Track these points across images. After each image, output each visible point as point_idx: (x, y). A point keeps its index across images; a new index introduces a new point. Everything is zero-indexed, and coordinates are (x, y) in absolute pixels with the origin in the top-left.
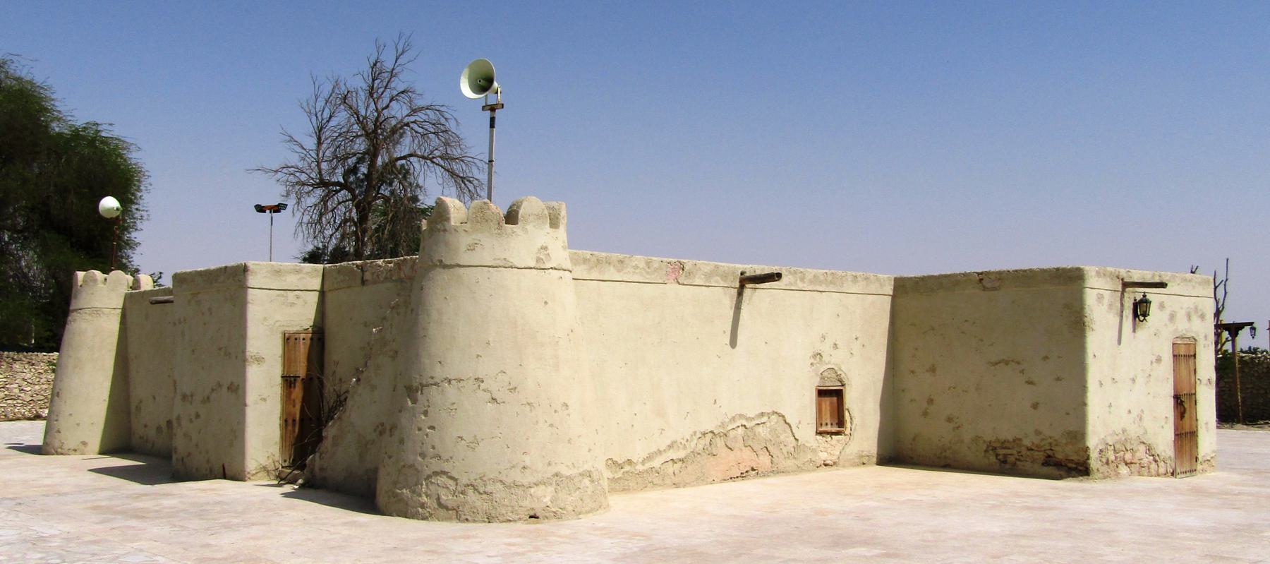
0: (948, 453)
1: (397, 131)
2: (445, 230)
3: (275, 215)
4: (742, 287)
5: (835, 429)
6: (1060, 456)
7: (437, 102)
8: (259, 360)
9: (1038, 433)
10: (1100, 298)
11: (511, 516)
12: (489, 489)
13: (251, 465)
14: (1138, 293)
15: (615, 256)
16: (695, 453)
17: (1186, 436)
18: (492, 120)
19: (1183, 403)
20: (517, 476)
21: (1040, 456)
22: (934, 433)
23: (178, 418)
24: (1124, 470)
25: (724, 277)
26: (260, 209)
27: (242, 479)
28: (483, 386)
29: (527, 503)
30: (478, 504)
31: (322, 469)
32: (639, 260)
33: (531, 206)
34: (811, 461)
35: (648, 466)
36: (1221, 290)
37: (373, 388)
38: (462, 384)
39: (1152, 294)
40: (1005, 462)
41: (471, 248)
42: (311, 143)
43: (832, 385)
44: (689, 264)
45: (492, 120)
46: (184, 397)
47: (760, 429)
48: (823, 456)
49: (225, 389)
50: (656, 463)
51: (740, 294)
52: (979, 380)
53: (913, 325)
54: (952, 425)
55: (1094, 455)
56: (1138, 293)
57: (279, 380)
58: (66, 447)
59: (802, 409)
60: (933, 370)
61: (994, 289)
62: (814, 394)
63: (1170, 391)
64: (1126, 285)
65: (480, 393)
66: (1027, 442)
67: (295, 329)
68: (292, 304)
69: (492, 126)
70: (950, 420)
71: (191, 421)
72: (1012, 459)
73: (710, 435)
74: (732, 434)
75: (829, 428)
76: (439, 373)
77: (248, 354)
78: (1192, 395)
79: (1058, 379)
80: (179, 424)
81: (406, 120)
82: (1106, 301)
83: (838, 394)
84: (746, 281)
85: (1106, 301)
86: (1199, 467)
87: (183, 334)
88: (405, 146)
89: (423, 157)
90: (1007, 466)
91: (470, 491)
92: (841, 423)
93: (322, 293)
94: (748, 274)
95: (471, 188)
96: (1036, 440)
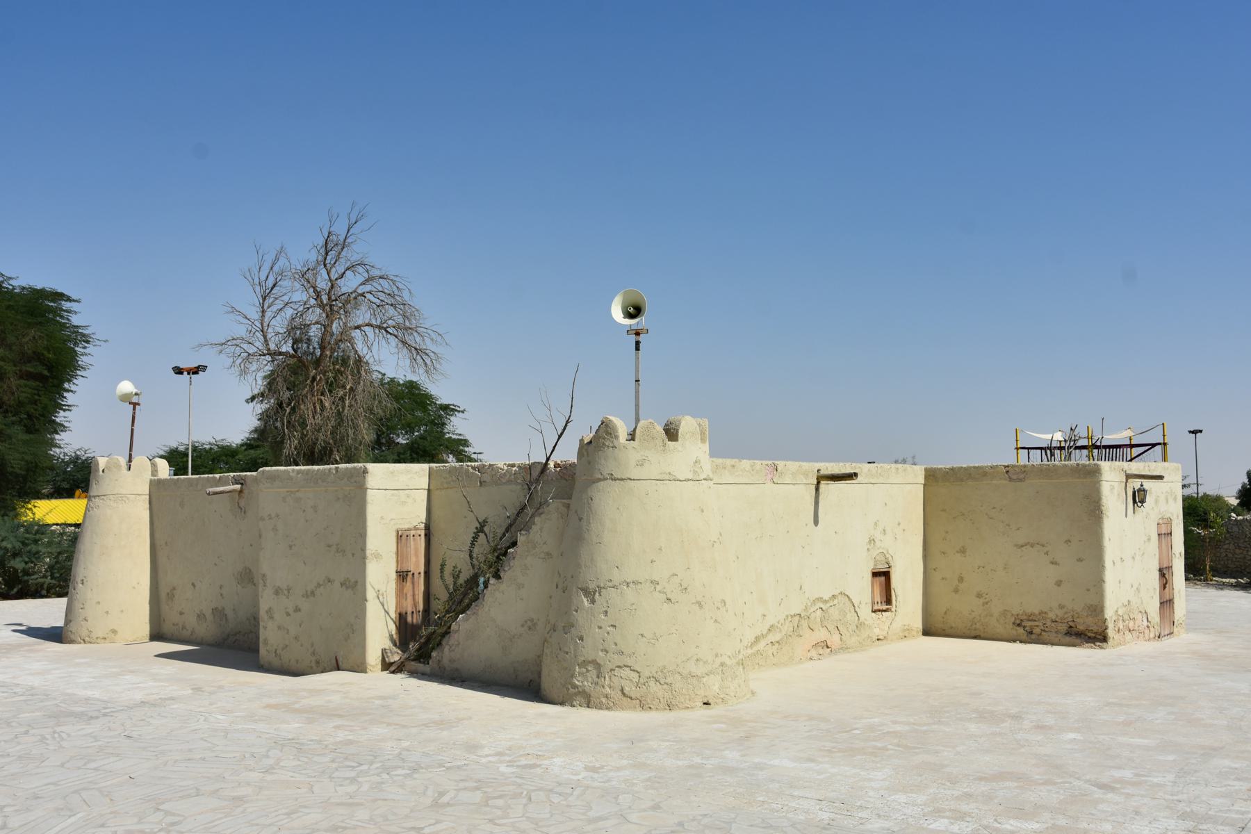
0: (978, 626)
1: (353, 299)
2: (614, 447)
3: (193, 376)
4: (818, 483)
5: (885, 607)
6: (1081, 628)
7: (391, 272)
8: (377, 556)
9: (1061, 607)
10: (1112, 488)
11: (688, 704)
12: (669, 680)
13: (373, 657)
14: (1136, 484)
15: (729, 462)
16: (788, 636)
17: (1167, 604)
18: (638, 343)
19: (1164, 574)
20: (692, 668)
21: (1064, 628)
22: (964, 607)
23: (269, 611)
24: (1128, 636)
25: (806, 474)
26: (179, 371)
27: (364, 671)
28: (659, 588)
29: (701, 692)
30: (660, 694)
31: (452, 661)
32: (746, 464)
33: (688, 425)
34: (869, 637)
35: (755, 649)
36: (332, 254)
37: (520, 586)
38: (639, 586)
39: (1148, 484)
40: (1031, 633)
41: (640, 464)
42: (254, 314)
43: (882, 567)
44: (781, 464)
45: (638, 343)
46: (277, 592)
47: (831, 610)
48: (877, 631)
49: (337, 584)
50: (761, 646)
51: (817, 489)
52: (1010, 560)
53: (944, 510)
54: (982, 600)
55: (1110, 625)
56: (1136, 484)
57: (394, 575)
58: (94, 635)
59: (863, 590)
60: (963, 551)
61: (1020, 480)
62: (870, 575)
63: (1155, 567)
64: (1128, 476)
65: (656, 594)
66: (1052, 615)
67: (406, 526)
68: (404, 503)
69: (637, 349)
70: (979, 596)
71: (288, 614)
72: (1037, 630)
73: (797, 618)
74: (812, 617)
75: (880, 607)
76: (617, 577)
77: (368, 552)
78: (1170, 568)
79: (1080, 560)
80: (271, 618)
81: (360, 291)
82: (1116, 492)
83: (886, 575)
84: (821, 478)
85: (1116, 492)
86: (1175, 630)
87: (275, 529)
88: (362, 315)
89: (380, 327)
90: (1033, 637)
91: (652, 683)
92: (888, 601)
93: (429, 490)
94: (822, 472)
95: (428, 362)
96: (1060, 613)
